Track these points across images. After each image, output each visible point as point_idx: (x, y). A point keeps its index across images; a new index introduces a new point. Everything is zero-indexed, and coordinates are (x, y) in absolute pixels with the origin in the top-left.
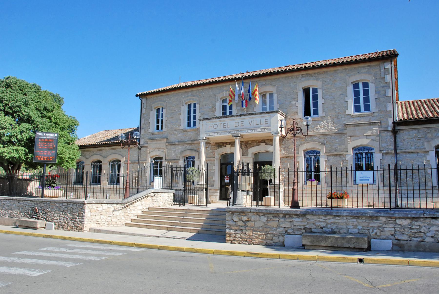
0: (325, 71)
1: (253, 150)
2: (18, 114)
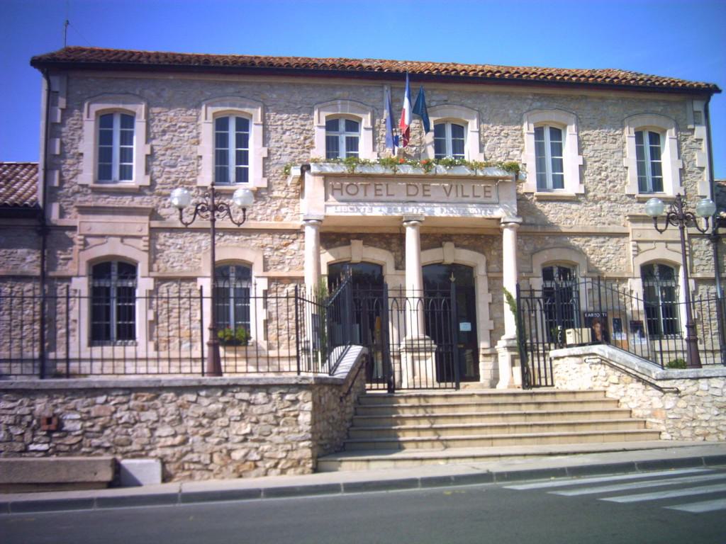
0: (582, 96)
1: (248, 246)
2: (156, 457)
